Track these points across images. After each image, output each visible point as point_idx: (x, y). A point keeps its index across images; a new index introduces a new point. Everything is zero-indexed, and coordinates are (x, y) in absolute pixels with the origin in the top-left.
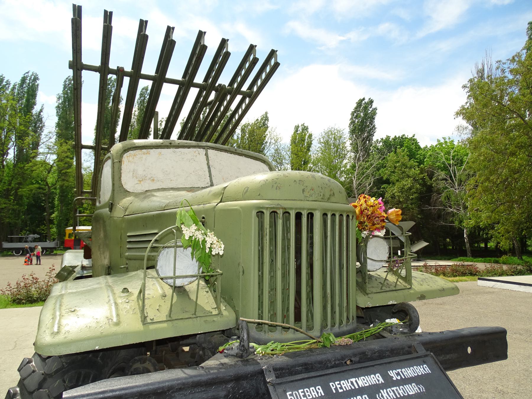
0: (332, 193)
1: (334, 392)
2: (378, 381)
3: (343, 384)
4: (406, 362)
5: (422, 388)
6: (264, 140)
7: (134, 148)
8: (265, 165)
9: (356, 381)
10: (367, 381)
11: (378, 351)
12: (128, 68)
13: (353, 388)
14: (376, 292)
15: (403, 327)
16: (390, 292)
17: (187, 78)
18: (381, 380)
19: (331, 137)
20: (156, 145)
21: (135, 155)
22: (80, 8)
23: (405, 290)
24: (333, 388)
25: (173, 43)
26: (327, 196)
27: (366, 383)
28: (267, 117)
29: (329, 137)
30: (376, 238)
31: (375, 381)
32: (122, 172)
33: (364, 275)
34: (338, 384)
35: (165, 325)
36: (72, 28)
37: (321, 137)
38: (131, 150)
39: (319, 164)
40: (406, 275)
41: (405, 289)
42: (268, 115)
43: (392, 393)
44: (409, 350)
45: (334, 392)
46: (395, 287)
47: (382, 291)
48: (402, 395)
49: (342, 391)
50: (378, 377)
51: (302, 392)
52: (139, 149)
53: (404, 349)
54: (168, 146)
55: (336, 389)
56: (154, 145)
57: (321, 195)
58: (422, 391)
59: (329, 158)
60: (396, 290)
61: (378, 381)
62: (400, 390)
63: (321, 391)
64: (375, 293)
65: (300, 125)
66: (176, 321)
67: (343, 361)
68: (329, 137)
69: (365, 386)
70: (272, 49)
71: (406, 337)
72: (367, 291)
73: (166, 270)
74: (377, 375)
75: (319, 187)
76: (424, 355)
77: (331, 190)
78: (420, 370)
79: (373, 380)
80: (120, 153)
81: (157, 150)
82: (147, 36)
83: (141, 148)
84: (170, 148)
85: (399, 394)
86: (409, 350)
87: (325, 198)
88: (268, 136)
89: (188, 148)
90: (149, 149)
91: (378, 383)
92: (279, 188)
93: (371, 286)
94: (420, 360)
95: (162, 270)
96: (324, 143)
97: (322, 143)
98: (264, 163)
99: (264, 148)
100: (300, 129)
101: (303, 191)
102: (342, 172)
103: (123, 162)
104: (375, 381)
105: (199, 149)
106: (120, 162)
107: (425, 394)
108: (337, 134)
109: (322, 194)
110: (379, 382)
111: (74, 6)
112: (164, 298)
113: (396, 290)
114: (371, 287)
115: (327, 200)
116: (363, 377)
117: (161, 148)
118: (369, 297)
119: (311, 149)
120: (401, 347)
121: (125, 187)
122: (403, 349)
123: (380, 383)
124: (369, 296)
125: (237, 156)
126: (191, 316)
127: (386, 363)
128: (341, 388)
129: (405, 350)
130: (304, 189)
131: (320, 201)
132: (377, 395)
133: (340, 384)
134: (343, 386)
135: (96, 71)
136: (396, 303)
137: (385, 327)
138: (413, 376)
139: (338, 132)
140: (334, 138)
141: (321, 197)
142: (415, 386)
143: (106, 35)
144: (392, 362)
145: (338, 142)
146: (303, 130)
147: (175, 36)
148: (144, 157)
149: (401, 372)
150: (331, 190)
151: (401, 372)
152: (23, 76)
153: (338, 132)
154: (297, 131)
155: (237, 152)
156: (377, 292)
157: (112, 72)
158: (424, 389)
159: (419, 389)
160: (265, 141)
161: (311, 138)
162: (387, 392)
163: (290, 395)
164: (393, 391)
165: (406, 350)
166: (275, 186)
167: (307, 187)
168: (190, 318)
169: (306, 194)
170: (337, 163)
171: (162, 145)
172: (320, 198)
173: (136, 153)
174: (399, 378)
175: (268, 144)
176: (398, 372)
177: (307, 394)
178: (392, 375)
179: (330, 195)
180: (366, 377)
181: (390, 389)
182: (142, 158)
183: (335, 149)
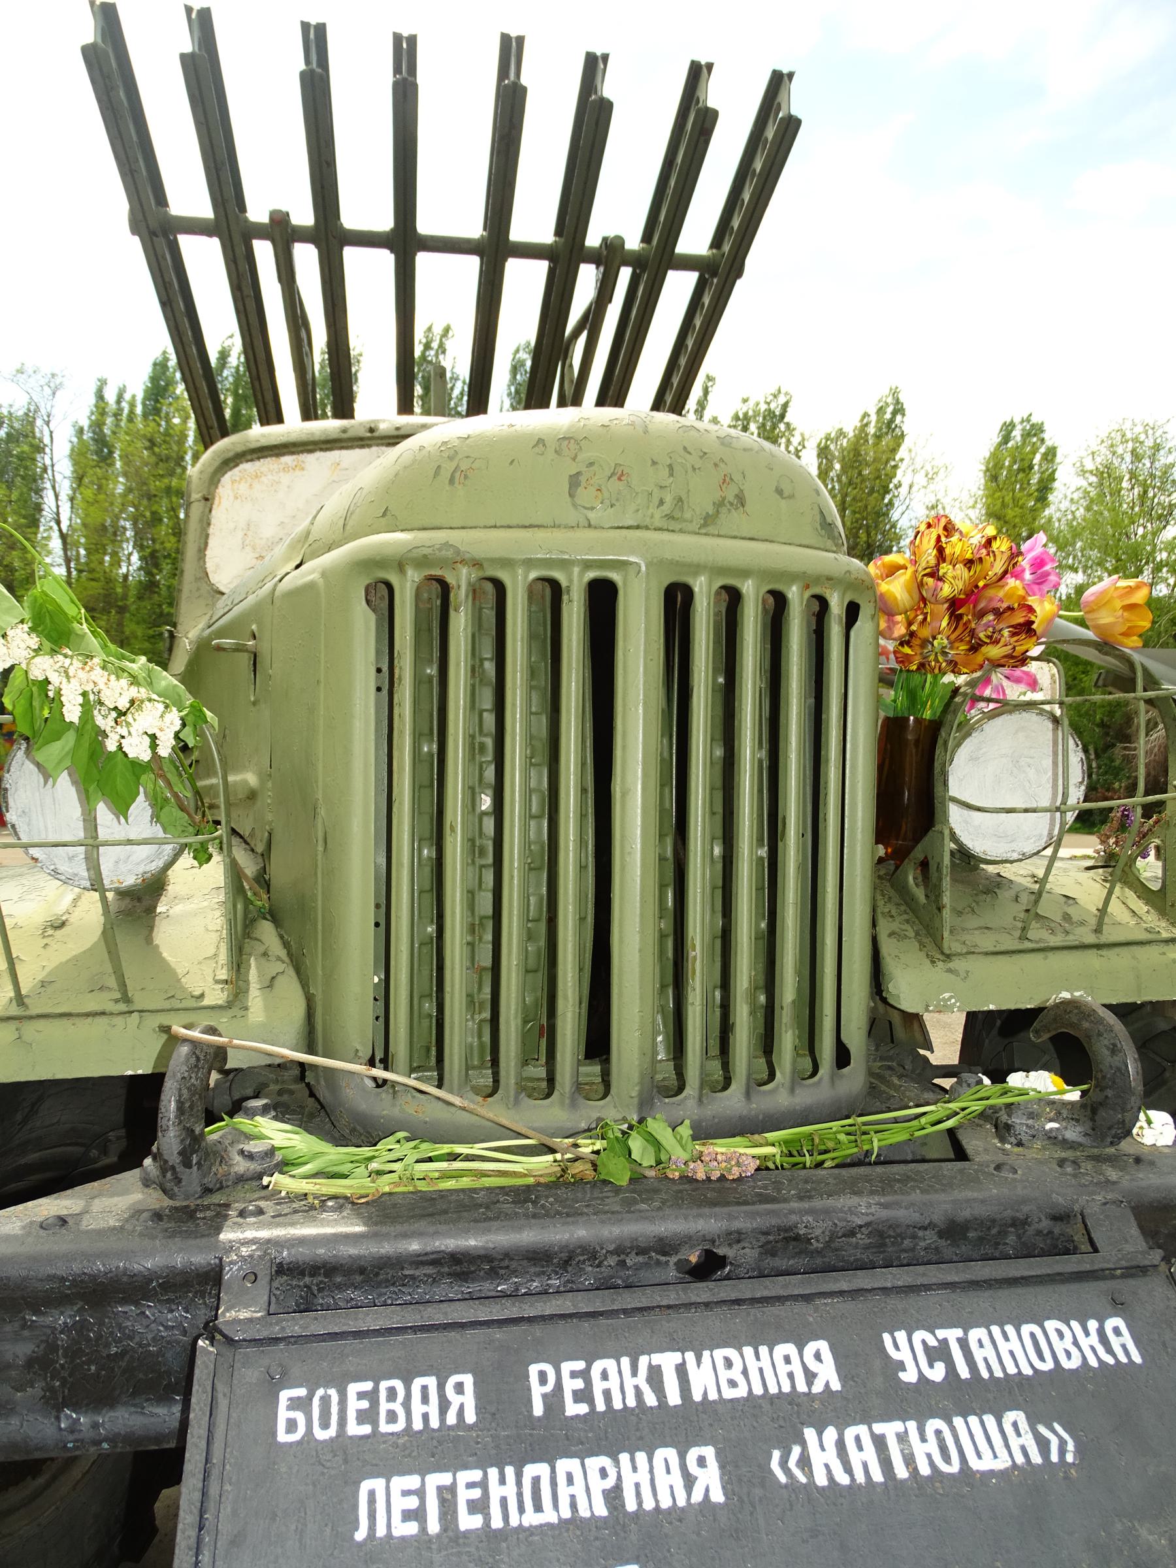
1: (538, 1409)
2: (810, 1376)
3: (605, 1376)
4: (1004, 1293)
5: (1062, 1444)
6: (891, 477)
9: (681, 1370)
10: (745, 1372)
11: (868, 1224)
12: (303, 215)
13: (651, 1400)
14: (992, 949)
15: (1065, 1113)
16: (1065, 952)
17: (726, 247)
18: (828, 1375)
19: (1120, 450)
20: (322, 438)
21: (257, 476)
22: (321, 29)
23: (1147, 948)
24: (538, 1392)
25: (605, 108)
26: (701, 501)
27: (733, 1384)
28: (898, 402)
29: (1114, 453)
30: (1016, 717)
31: (791, 1376)
32: (211, 531)
33: (936, 874)
34: (574, 1375)
37: (1084, 454)
38: (247, 461)
39: (1079, 544)
40: (1164, 883)
41: (1149, 942)
42: (900, 396)
43: (870, 1454)
44: (1057, 1231)
45: (538, 1409)
46: (1098, 930)
47: (1028, 945)
48: (925, 1470)
49: (583, 1409)
50: (818, 1356)
51: (361, 1396)
52: (271, 456)
53: (1025, 1222)
54: (362, 439)
55: (554, 1400)
56: (317, 438)
57: (661, 502)
58: (1054, 1458)
59: (1115, 524)
60: (1098, 947)
61: (810, 1376)
62: (923, 1439)
63: (469, 1400)
64: (987, 954)
65: (1017, 420)
66: (42, 1022)
67: (670, 1255)
68: (1114, 453)
69: (483, 1467)
71: (1061, 1163)
72: (946, 944)
73: (46, 827)
74: (811, 1348)
75: (654, 463)
76: (1124, 1263)
77: (727, 480)
78: (1076, 1343)
79: (783, 1369)
80: (211, 470)
81: (328, 454)
83: (277, 451)
84: (369, 446)
85: (909, 1460)
86: (1057, 1231)
87: (688, 515)
88: (903, 466)
90: (302, 452)
91: (802, 1387)
92: (466, 477)
93: (982, 924)
94: (1090, 1290)
95: (29, 825)
96: (1099, 474)
97: (1091, 472)
99: (891, 503)
100: (1017, 434)
101: (574, 482)
102: (1158, 568)
103: (217, 499)
104: (791, 1376)
106: (207, 499)
107: (1067, 1477)
108: (1142, 437)
109: (668, 499)
110: (810, 1383)
112: (50, 932)
113: (1098, 947)
114: (980, 928)
115: (705, 525)
116: (731, 1353)
118: (950, 971)
119: (1051, 498)
120: (1009, 1213)
121: (214, 578)
122: (1020, 1224)
123: (818, 1388)
124: (956, 964)
126: (110, 1007)
127: (884, 1290)
128: (585, 1395)
129: (1031, 1231)
130: (579, 474)
131: (660, 529)
132: (776, 1455)
133: (585, 1374)
134: (598, 1387)
135: (210, 235)
137: (991, 1107)
138: (1027, 1371)
139: (1146, 432)
140: (1133, 452)
141: (666, 508)
142: (1023, 1425)
143: (197, 93)
144: (927, 1287)
145: (1148, 465)
146: (1027, 435)
147: (714, 95)
148: (285, 478)
149: (963, 1343)
150: (727, 480)
151: (963, 1343)
152: (220, 348)
153: (1146, 432)
154: (1006, 439)
156: (997, 949)
157: (261, 232)
158: (1071, 1446)
159: (1043, 1445)
160: (895, 481)
161: (1052, 461)
162: (841, 1445)
163: (295, 1404)
164: (880, 1443)
165: (1039, 1233)
166: (449, 467)
167: (591, 464)
168: (103, 1013)
170: (1144, 537)
171: (345, 436)
172: (657, 516)
173: (262, 469)
174: (937, 1373)
175: (903, 490)
176: (944, 1342)
177: (384, 1406)
178: (904, 1355)
179: (720, 504)
180: (748, 1351)
181: (862, 1430)
182: (279, 483)
183: (1136, 491)
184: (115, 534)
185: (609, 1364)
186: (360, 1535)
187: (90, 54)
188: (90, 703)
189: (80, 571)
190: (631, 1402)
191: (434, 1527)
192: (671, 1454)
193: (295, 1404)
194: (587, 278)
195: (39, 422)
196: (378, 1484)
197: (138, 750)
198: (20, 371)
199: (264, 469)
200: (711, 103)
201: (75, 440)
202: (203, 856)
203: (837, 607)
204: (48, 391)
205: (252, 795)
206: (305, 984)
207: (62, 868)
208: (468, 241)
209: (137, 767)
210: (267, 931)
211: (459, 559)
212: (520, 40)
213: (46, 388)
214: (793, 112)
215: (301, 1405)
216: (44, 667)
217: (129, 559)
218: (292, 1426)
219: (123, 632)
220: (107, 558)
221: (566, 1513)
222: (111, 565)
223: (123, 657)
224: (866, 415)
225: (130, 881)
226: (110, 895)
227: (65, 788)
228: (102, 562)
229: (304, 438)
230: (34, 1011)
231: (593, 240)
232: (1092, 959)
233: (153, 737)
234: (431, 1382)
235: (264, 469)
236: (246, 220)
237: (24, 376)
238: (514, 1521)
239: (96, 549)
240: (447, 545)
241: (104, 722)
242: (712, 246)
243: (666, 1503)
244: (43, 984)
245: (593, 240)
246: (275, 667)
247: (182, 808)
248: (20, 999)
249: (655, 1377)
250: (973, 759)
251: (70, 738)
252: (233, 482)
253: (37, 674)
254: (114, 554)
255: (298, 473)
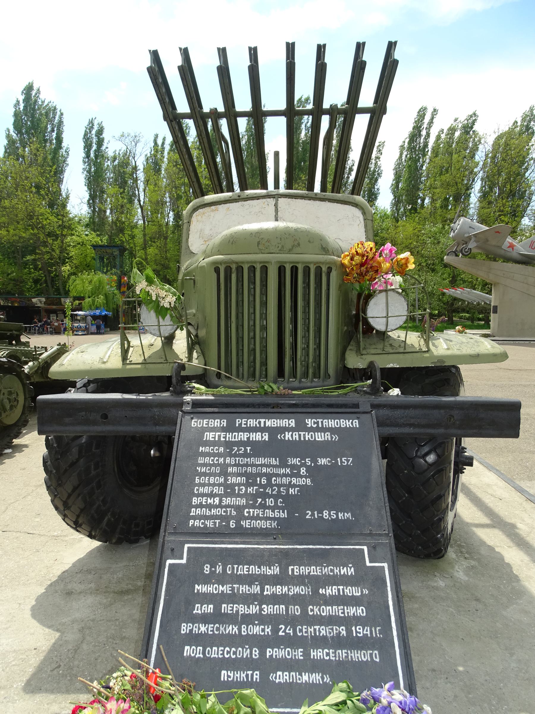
0: (296, 243)
1: (237, 425)
7: (202, 205)
8: (357, 209)
12: (221, 109)
13: (258, 425)
35: (139, 366)
36: (151, 78)
43: (297, 437)
45: (237, 425)
47: (384, 352)
54: (236, 199)
56: (222, 200)
70: (389, 42)
80: (190, 212)
81: (226, 205)
82: (326, 64)
84: (238, 202)
87: (285, 249)
89: (257, 199)
98: (356, 207)
105: (268, 200)
109: (280, 246)
111: (219, 49)
116: (275, 420)
117: (230, 203)
121: (191, 248)
123: (290, 426)
124: (364, 357)
125: (318, 203)
126: (163, 362)
128: (246, 424)
133: (247, 421)
134: (249, 423)
136: (398, 366)
141: (279, 248)
148: (212, 214)
150: (295, 240)
155: (317, 197)
159: (332, 438)
163: (195, 422)
166: (232, 240)
168: (162, 363)
169: (261, 247)
177: (210, 423)
184: (162, 204)
185: (252, 420)
186: (205, 439)
187: (150, 70)
188: (158, 296)
189: (148, 222)
190: (254, 426)
191: (217, 439)
192: (260, 434)
193: (195, 422)
194: (325, 121)
195: (131, 158)
196: (208, 433)
197: (167, 305)
198: (123, 136)
199: (206, 211)
200: (364, 59)
201: (145, 163)
202: (182, 329)
203: (324, 269)
204: (133, 144)
205: (194, 315)
206: (204, 358)
207: (152, 332)
208: (281, 111)
209: (167, 309)
210: (197, 347)
211: (233, 262)
212: (293, 44)
213: (133, 142)
214: (395, 58)
215: (196, 422)
216: (148, 289)
217: (168, 216)
218: (194, 424)
219: (166, 247)
220: (159, 216)
221: (239, 439)
222: (161, 218)
223: (164, 285)
224: (516, 122)
225: (167, 335)
226: (163, 338)
227: (153, 314)
228: (157, 218)
229: (218, 200)
230: (148, 362)
231: (326, 105)
232: (401, 356)
233: (170, 303)
234: (219, 420)
235: (206, 211)
236: (202, 112)
237: (124, 138)
238: (230, 440)
239: (155, 211)
240: (230, 259)
241: (161, 300)
242: (374, 104)
243: (257, 440)
244: (149, 357)
245: (326, 105)
246: (198, 284)
247: (177, 318)
248: (145, 359)
249: (260, 423)
250: (375, 304)
251: (153, 303)
252: (197, 216)
253: (147, 290)
254: (162, 213)
255: (216, 212)
